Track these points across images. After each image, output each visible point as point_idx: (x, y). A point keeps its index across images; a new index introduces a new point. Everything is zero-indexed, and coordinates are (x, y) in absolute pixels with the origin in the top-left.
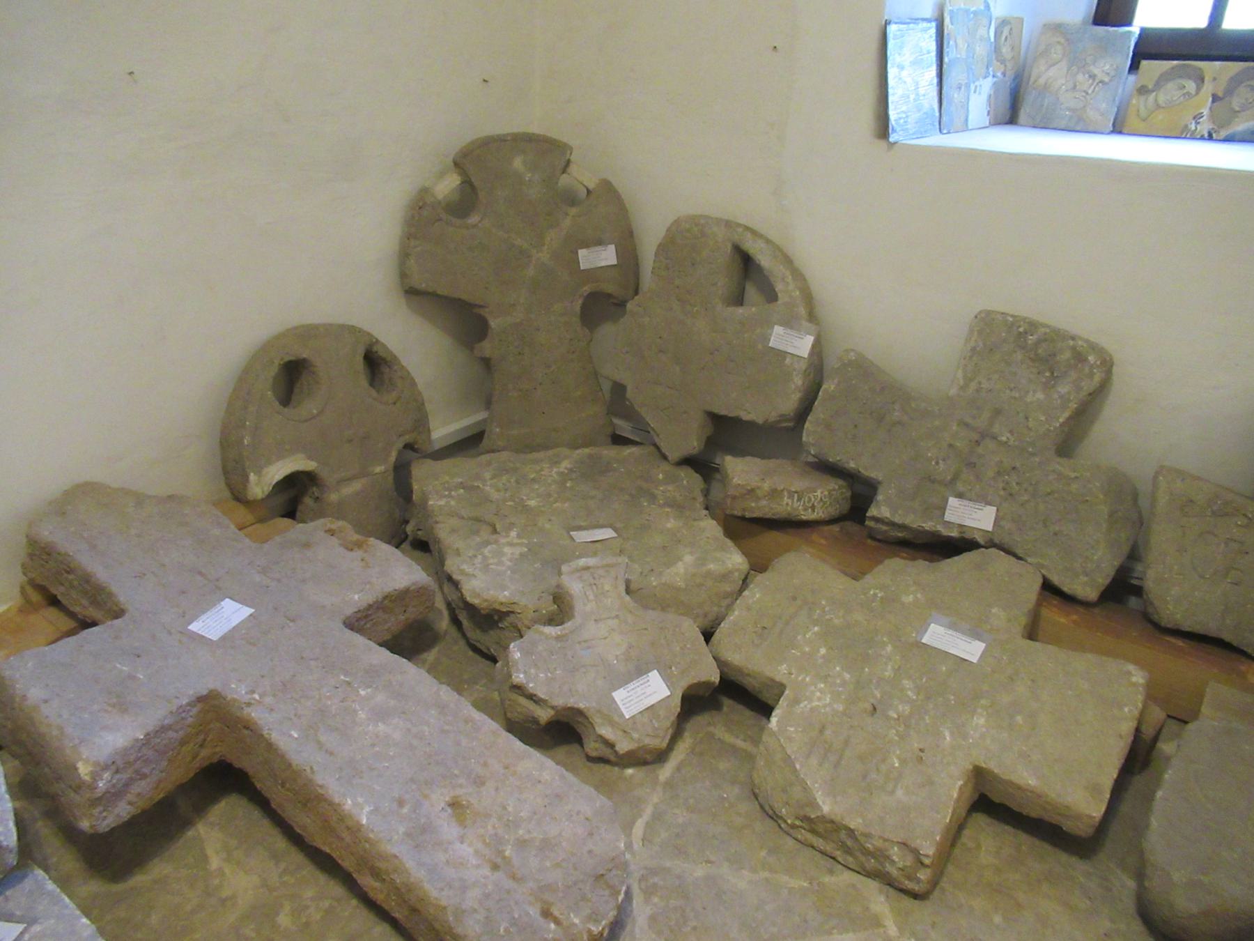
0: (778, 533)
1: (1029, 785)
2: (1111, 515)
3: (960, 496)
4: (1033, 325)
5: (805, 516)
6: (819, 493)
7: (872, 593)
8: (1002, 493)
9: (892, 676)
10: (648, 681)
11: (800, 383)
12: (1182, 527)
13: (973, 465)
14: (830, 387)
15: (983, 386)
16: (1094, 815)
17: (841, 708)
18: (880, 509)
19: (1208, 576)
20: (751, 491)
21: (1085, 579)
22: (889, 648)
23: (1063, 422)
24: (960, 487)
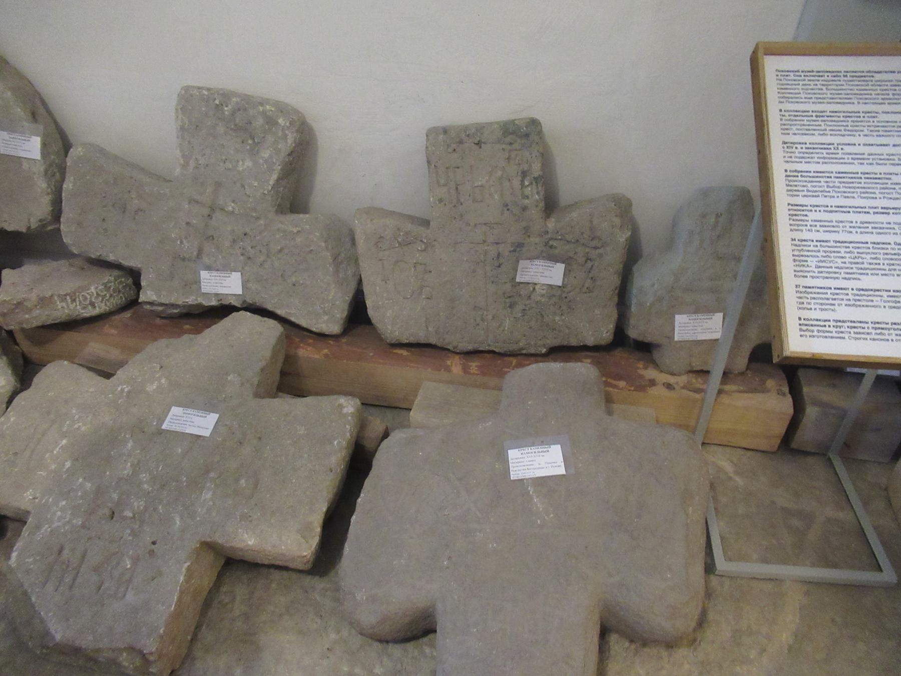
0: (71, 333)
1: (248, 545)
2: (335, 258)
3: (209, 268)
4: (226, 96)
5: (87, 313)
6: (93, 289)
7: (119, 389)
8: (242, 258)
9: (130, 473)
10: (553, 267)
11: (44, 185)
12: (380, 260)
13: (211, 238)
14: (69, 186)
15: (200, 162)
16: (305, 554)
17: (79, 522)
18: (147, 295)
19: (409, 297)
20: (19, 304)
21: (326, 318)
22: (130, 444)
23: (274, 185)
24: (206, 260)
